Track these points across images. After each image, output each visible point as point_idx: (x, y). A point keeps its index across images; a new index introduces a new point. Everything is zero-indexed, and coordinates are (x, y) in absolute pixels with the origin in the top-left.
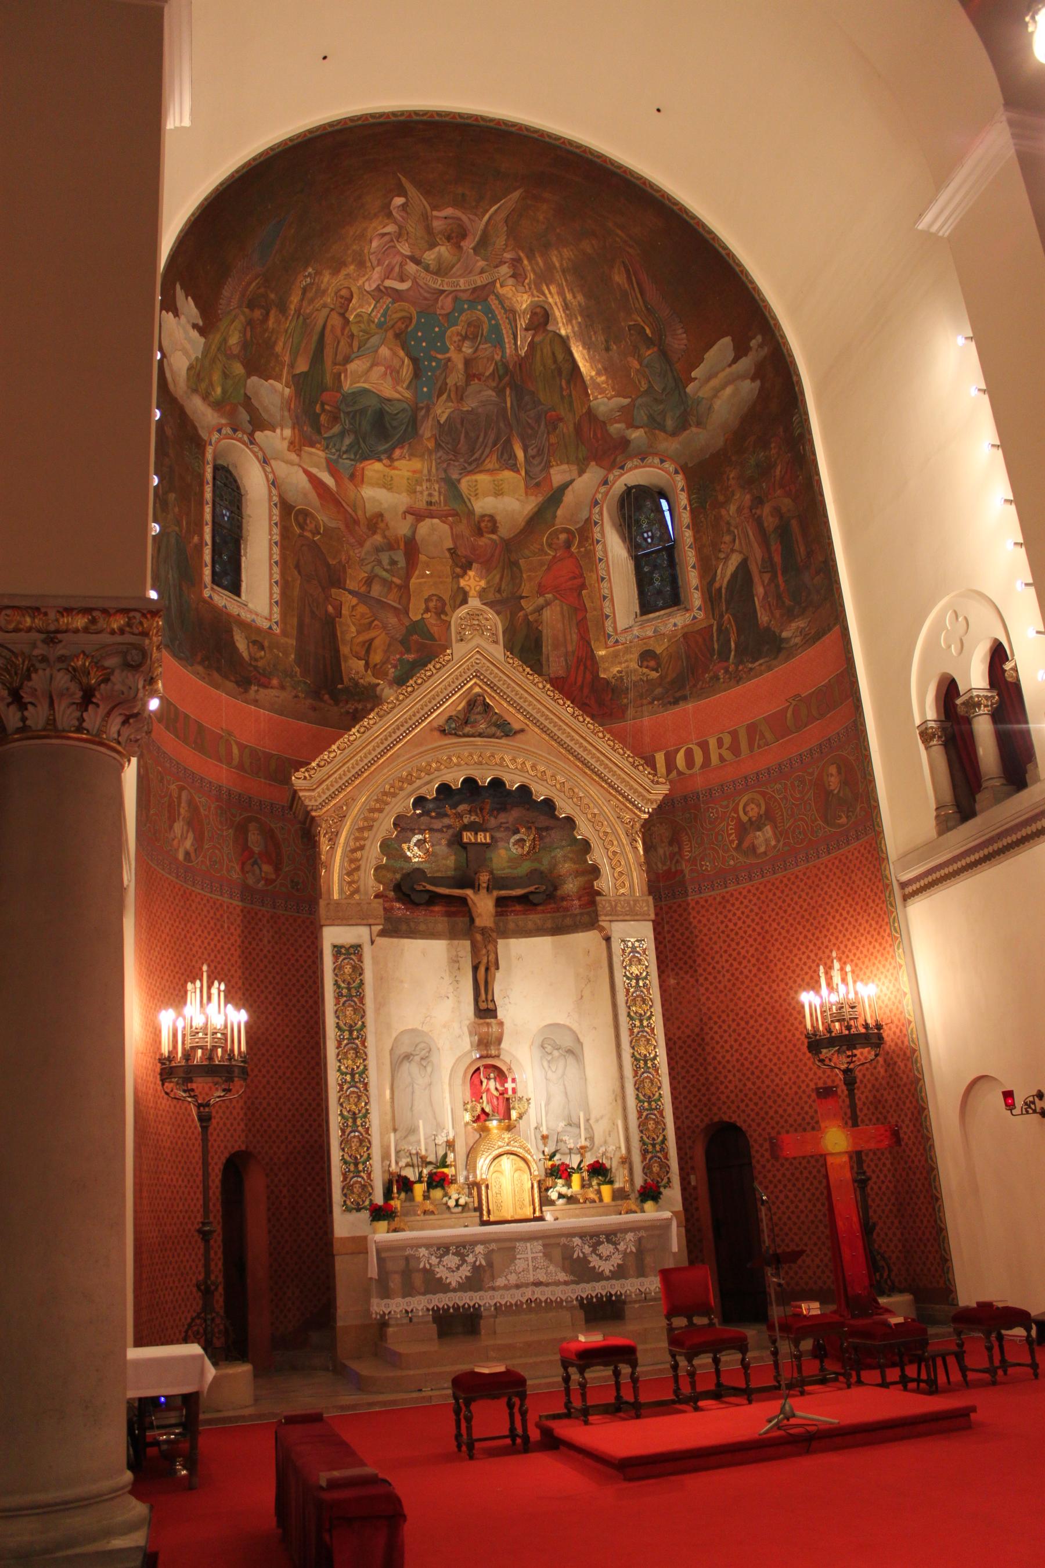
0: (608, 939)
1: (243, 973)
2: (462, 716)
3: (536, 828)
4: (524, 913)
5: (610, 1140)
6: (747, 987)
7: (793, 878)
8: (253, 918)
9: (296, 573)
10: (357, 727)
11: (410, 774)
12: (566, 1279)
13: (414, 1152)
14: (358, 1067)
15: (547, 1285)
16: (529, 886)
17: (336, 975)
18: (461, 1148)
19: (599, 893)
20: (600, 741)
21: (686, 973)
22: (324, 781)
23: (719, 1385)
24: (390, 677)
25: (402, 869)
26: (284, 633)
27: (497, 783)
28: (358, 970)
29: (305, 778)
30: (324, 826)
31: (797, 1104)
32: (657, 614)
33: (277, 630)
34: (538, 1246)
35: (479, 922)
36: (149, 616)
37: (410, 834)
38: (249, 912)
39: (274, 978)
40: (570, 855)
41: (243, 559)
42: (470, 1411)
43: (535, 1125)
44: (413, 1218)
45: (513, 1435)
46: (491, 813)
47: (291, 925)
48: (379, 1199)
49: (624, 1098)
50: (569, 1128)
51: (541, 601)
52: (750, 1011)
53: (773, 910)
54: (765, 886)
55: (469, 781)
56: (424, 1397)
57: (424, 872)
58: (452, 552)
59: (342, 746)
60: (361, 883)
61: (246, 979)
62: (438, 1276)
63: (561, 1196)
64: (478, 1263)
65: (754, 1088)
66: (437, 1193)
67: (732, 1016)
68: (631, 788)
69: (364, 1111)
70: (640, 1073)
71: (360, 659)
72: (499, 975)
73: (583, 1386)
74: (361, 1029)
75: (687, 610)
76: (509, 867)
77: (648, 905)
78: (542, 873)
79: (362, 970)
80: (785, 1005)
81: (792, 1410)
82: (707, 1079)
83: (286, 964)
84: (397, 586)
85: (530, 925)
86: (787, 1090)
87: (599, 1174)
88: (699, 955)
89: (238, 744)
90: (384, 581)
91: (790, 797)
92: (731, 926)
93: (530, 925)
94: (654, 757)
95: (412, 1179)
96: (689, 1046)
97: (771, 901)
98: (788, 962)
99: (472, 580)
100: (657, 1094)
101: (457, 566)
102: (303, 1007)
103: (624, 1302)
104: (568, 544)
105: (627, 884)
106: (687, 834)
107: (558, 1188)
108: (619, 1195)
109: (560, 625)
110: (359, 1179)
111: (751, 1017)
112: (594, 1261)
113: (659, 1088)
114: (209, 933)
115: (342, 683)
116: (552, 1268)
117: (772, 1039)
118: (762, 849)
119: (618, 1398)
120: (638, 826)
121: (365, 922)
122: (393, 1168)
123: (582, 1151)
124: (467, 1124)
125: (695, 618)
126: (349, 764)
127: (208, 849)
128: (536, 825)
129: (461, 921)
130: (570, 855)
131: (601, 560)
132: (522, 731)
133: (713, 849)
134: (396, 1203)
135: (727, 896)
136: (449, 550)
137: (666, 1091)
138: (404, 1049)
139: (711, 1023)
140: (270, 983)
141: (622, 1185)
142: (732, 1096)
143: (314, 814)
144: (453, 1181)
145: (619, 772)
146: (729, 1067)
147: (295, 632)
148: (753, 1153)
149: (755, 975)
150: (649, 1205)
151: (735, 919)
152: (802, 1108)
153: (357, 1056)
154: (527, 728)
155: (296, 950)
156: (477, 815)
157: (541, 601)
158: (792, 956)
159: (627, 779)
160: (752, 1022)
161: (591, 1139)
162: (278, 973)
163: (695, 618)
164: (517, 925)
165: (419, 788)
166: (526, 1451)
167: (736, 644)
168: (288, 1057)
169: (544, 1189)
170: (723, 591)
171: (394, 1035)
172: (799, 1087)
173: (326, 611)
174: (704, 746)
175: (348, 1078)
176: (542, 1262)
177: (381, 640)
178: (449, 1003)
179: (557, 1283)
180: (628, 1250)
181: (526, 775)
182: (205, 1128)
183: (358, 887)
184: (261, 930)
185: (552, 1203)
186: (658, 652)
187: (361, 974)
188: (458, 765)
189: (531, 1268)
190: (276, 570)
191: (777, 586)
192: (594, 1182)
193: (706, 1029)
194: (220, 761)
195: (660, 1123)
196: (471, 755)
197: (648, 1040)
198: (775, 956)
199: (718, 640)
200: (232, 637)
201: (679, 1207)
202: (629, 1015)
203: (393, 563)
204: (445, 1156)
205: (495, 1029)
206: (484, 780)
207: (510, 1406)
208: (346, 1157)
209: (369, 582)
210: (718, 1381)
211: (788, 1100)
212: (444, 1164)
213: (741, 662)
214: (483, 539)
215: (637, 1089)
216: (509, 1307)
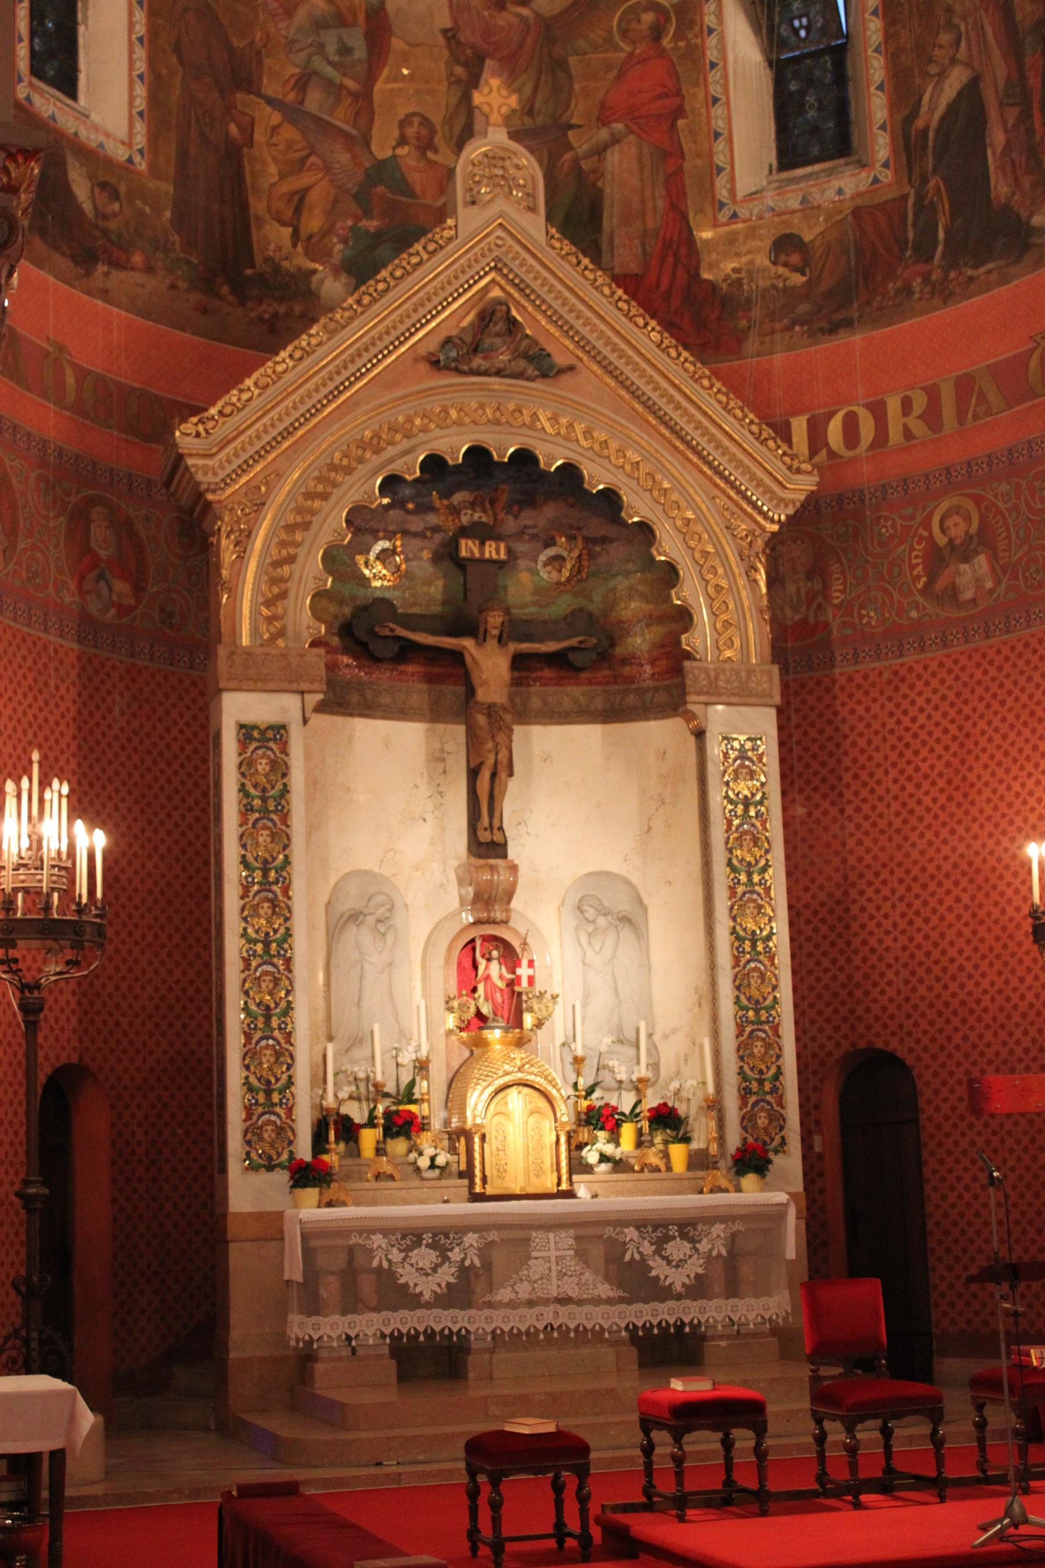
0: (700, 735)
1: (79, 765)
2: (468, 339)
3: (584, 538)
4: (559, 682)
5: (685, 1070)
6: (929, 827)
7: (1020, 647)
8: (97, 672)
9: (174, 60)
10: (290, 348)
11: (376, 435)
12: (611, 1294)
13: (362, 1075)
14: (276, 931)
15: (580, 1302)
16: (569, 638)
17: (243, 775)
18: (439, 1074)
19: (688, 656)
20: (704, 393)
21: (825, 796)
22: (230, 442)
23: (889, 1470)
24: (336, 259)
25: (354, 598)
26: (154, 170)
27: (524, 458)
28: (280, 768)
29: (198, 435)
30: (227, 519)
31: (1003, 1027)
32: (809, 169)
33: (141, 165)
34: (567, 1238)
35: (481, 695)
36: (20, 160)
37: (369, 538)
38: (90, 661)
39: (130, 775)
40: (640, 588)
41: (81, 29)
42: (499, 1493)
43: (562, 1040)
44: (358, 1185)
45: (560, 1533)
46: (508, 510)
47: (159, 685)
48: (304, 1150)
49: (714, 1001)
50: (618, 1047)
51: (603, 134)
52: (931, 869)
53: (981, 699)
54: (970, 658)
55: (478, 454)
56: (388, 1475)
57: (392, 605)
58: (450, 35)
59: (263, 381)
60: (289, 621)
61: (84, 774)
62: (402, 1281)
63: (604, 1158)
64: (467, 1263)
65: (930, 996)
66: (398, 1146)
67: (899, 873)
68: (753, 477)
69: (283, 1004)
70: (743, 961)
71: (283, 224)
72: (513, 786)
73: (678, 1460)
74: (283, 868)
75: (862, 165)
76: (534, 603)
77: (770, 680)
78: (591, 615)
79: (287, 768)
80: (992, 861)
81: (1024, 1514)
82: (850, 977)
83: (149, 753)
84: (350, 93)
85: (567, 703)
86: (986, 1001)
87: (666, 1126)
88: (847, 769)
89: (77, 368)
90: (329, 84)
91: (1023, 507)
92: (906, 721)
93: (567, 703)
94: (788, 425)
95: (357, 1120)
96: (823, 921)
97: (979, 683)
98: (1002, 789)
99: (495, 94)
100: (770, 998)
101: (457, 61)
102: (177, 825)
103: (704, 1338)
104: (657, 33)
105: (737, 643)
106: (839, 561)
107: (599, 1146)
108: (699, 1161)
109: (635, 181)
110: (273, 1118)
111: (932, 877)
112: (658, 1268)
113: (775, 988)
114: (25, 696)
115: (253, 266)
116: (588, 1276)
117: (966, 916)
118: (969, 595)
119: (728, 1482)
120: (760, 543)
121: (294, 686)
122: (330, 1101)
123: (639, 1086)
124: (450, 1032)
125: (876, 180)
126: (274, 414)
127: (25, 550)
128: (585, 532)
129: (452, 692)
130: (640, 588)
131: (713, 65)
132: (571, 368)
133: (885, 591)
134: (331, 1158)
135: (903, 672)
136: (444, 32)
137: (785, 994)
138: (348, 904)
139: (862, 884)
140: (124, 783)
141: (703, 1146)
142: (892, 1008)
143: (210, 497)
144: (424, 1127)
145: (733, 449)
146: (889, 958)
147: (172, 171)
148: (922, 1103)
149: (943, 808)
150: (749, 1181)
151: (913, 711)
152: (1011, 1034)
153: (274, 913)
154: (579, 364)
155: (168, 730)
156: (484, 510)
157: (603, 134)
158: (1008, 779)
159: (747, 461)
160: (932, 886)
161: (655, 1066)
162: (136, 767)
163: (876, 180)
164: (545, 703)
165: (392, 460)
166: (586, 1559)
167: (947, 232)
168: (149, 910)
169: (577, 1147)
170: (931, 135)
171: (333, 880)
172: (1008, 999)
173: (227, 134)
174: (878, 410)
175: (259, 947)
176: (572, 1264)
177: (320, 194)
178: (427, 830)
179: (597, 1301)
180: (715, 1253)
181: (573, 446)
182: (32, 1027)
183: (284, 627)
184: (109, 693)
185: (588, 1169)
186: (807, 237)
187: (284, 775)
188: (459, 423)
189: (554, 1274)
190: (140, 53)
191: (1030, 131)
192: (658, 1139)
193: (853, 893)
194: (45, 396)
195: (773, 1045)
196: (482, 407)
197: (760, 907)
198: (979, 777)
199: (914, 224)
200: (65, 174)
201: (799, 1186)
202: (729, 863)
203: (345, 50)
204: (412, 1084)
205: (503, 876)
206: (502, 451)
207: (558, 1488)
208: (253, 1079)
209: (302, 83)
210: (888, 1464)
211: (987, 1019)
212: (409, 1096)
213: (953, 265)
214: (505, 14)
215: (738, 988)
216: (515, 1336)
